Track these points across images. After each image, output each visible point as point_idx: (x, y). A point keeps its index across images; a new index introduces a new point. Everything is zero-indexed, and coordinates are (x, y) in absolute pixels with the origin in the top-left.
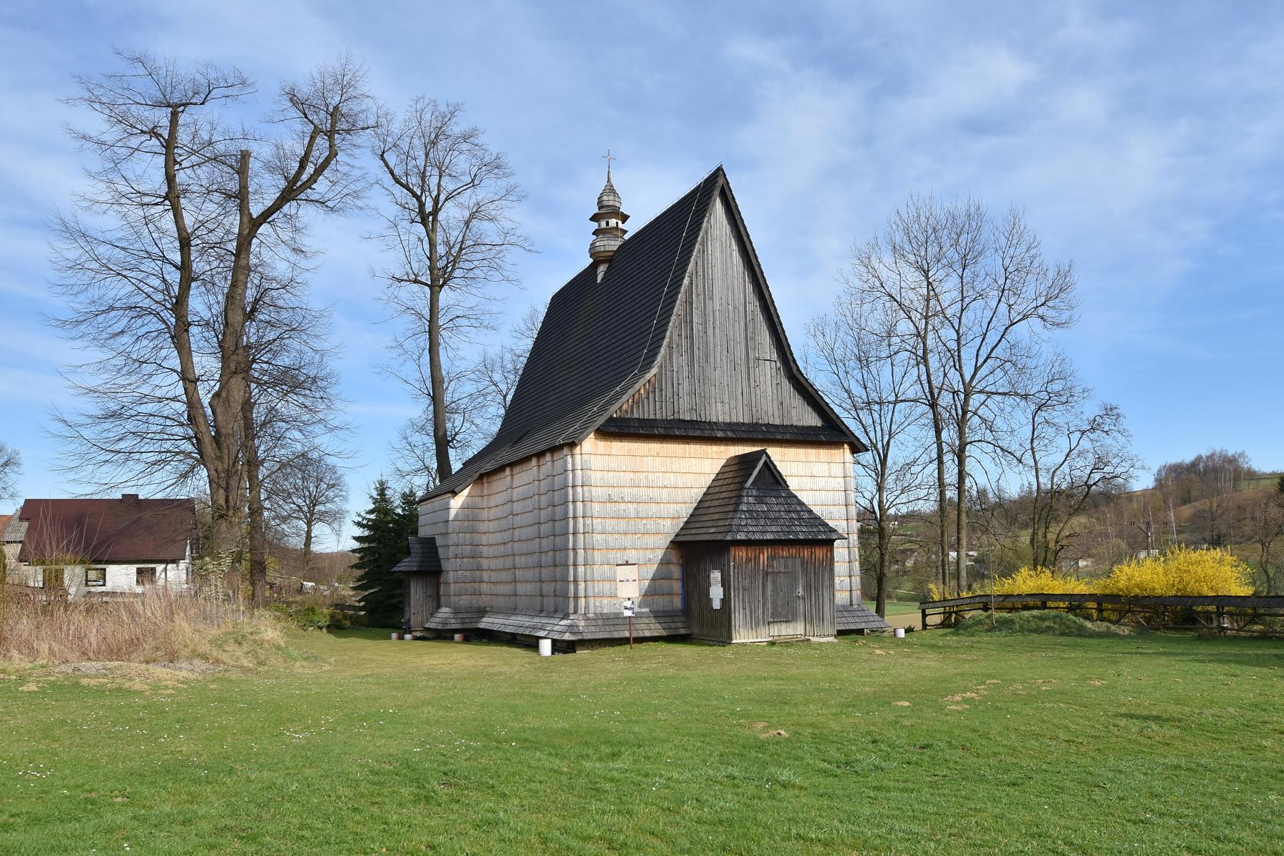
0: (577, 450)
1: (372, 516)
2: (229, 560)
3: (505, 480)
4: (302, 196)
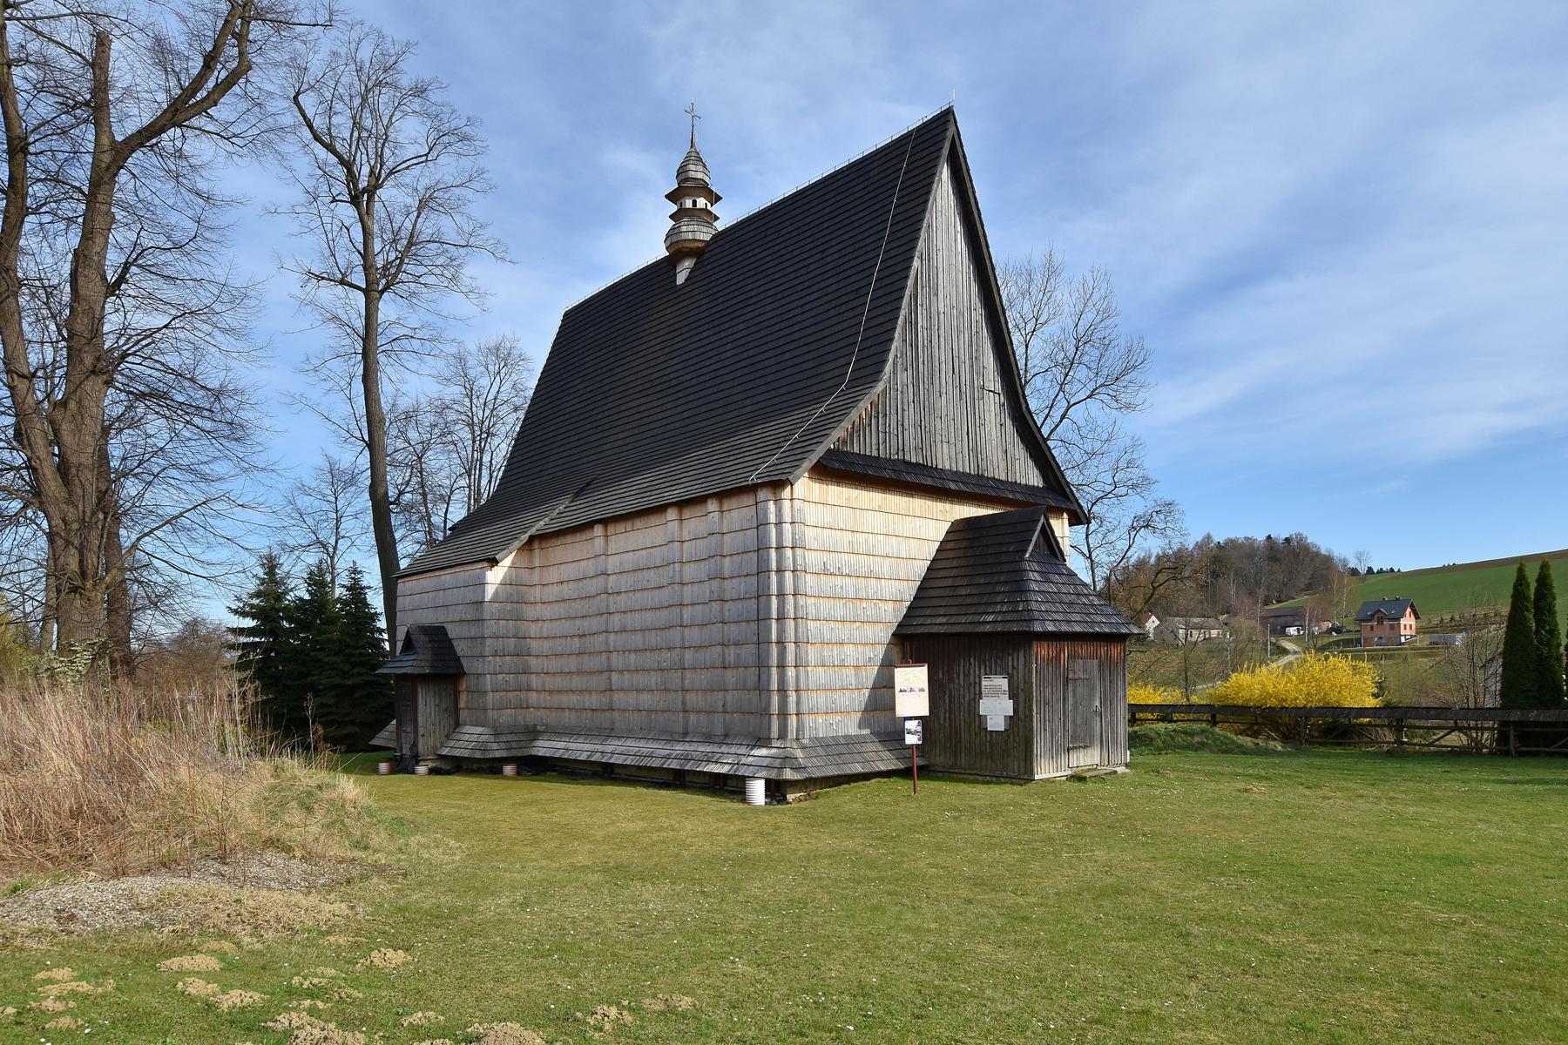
0: (786, 493)
1: (255, 601)
2: (88, 655)
3: (564, 551)
4: (195, 122)
